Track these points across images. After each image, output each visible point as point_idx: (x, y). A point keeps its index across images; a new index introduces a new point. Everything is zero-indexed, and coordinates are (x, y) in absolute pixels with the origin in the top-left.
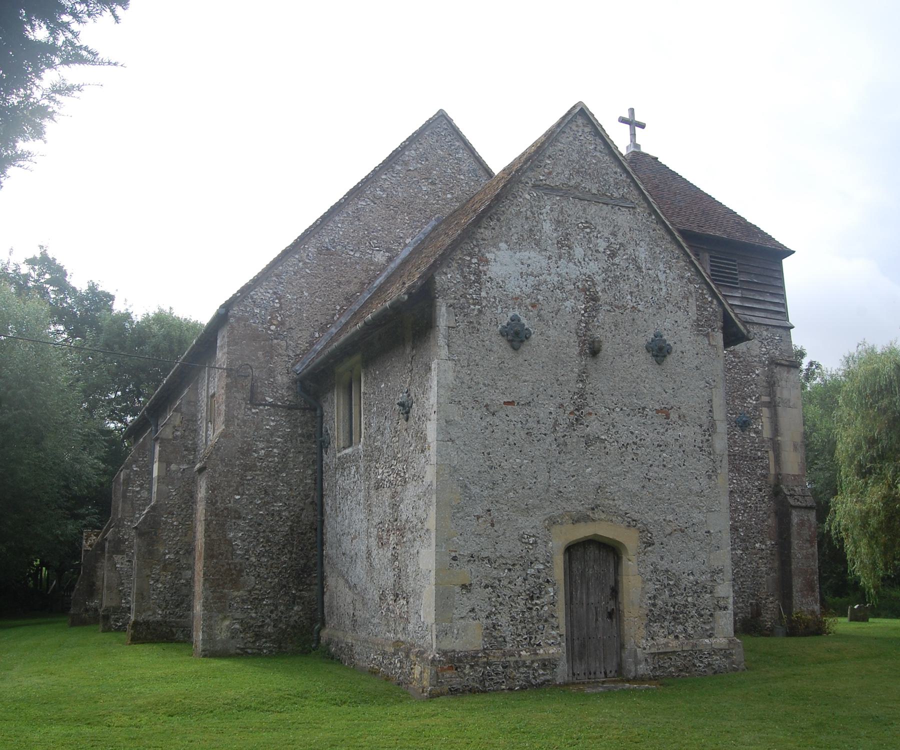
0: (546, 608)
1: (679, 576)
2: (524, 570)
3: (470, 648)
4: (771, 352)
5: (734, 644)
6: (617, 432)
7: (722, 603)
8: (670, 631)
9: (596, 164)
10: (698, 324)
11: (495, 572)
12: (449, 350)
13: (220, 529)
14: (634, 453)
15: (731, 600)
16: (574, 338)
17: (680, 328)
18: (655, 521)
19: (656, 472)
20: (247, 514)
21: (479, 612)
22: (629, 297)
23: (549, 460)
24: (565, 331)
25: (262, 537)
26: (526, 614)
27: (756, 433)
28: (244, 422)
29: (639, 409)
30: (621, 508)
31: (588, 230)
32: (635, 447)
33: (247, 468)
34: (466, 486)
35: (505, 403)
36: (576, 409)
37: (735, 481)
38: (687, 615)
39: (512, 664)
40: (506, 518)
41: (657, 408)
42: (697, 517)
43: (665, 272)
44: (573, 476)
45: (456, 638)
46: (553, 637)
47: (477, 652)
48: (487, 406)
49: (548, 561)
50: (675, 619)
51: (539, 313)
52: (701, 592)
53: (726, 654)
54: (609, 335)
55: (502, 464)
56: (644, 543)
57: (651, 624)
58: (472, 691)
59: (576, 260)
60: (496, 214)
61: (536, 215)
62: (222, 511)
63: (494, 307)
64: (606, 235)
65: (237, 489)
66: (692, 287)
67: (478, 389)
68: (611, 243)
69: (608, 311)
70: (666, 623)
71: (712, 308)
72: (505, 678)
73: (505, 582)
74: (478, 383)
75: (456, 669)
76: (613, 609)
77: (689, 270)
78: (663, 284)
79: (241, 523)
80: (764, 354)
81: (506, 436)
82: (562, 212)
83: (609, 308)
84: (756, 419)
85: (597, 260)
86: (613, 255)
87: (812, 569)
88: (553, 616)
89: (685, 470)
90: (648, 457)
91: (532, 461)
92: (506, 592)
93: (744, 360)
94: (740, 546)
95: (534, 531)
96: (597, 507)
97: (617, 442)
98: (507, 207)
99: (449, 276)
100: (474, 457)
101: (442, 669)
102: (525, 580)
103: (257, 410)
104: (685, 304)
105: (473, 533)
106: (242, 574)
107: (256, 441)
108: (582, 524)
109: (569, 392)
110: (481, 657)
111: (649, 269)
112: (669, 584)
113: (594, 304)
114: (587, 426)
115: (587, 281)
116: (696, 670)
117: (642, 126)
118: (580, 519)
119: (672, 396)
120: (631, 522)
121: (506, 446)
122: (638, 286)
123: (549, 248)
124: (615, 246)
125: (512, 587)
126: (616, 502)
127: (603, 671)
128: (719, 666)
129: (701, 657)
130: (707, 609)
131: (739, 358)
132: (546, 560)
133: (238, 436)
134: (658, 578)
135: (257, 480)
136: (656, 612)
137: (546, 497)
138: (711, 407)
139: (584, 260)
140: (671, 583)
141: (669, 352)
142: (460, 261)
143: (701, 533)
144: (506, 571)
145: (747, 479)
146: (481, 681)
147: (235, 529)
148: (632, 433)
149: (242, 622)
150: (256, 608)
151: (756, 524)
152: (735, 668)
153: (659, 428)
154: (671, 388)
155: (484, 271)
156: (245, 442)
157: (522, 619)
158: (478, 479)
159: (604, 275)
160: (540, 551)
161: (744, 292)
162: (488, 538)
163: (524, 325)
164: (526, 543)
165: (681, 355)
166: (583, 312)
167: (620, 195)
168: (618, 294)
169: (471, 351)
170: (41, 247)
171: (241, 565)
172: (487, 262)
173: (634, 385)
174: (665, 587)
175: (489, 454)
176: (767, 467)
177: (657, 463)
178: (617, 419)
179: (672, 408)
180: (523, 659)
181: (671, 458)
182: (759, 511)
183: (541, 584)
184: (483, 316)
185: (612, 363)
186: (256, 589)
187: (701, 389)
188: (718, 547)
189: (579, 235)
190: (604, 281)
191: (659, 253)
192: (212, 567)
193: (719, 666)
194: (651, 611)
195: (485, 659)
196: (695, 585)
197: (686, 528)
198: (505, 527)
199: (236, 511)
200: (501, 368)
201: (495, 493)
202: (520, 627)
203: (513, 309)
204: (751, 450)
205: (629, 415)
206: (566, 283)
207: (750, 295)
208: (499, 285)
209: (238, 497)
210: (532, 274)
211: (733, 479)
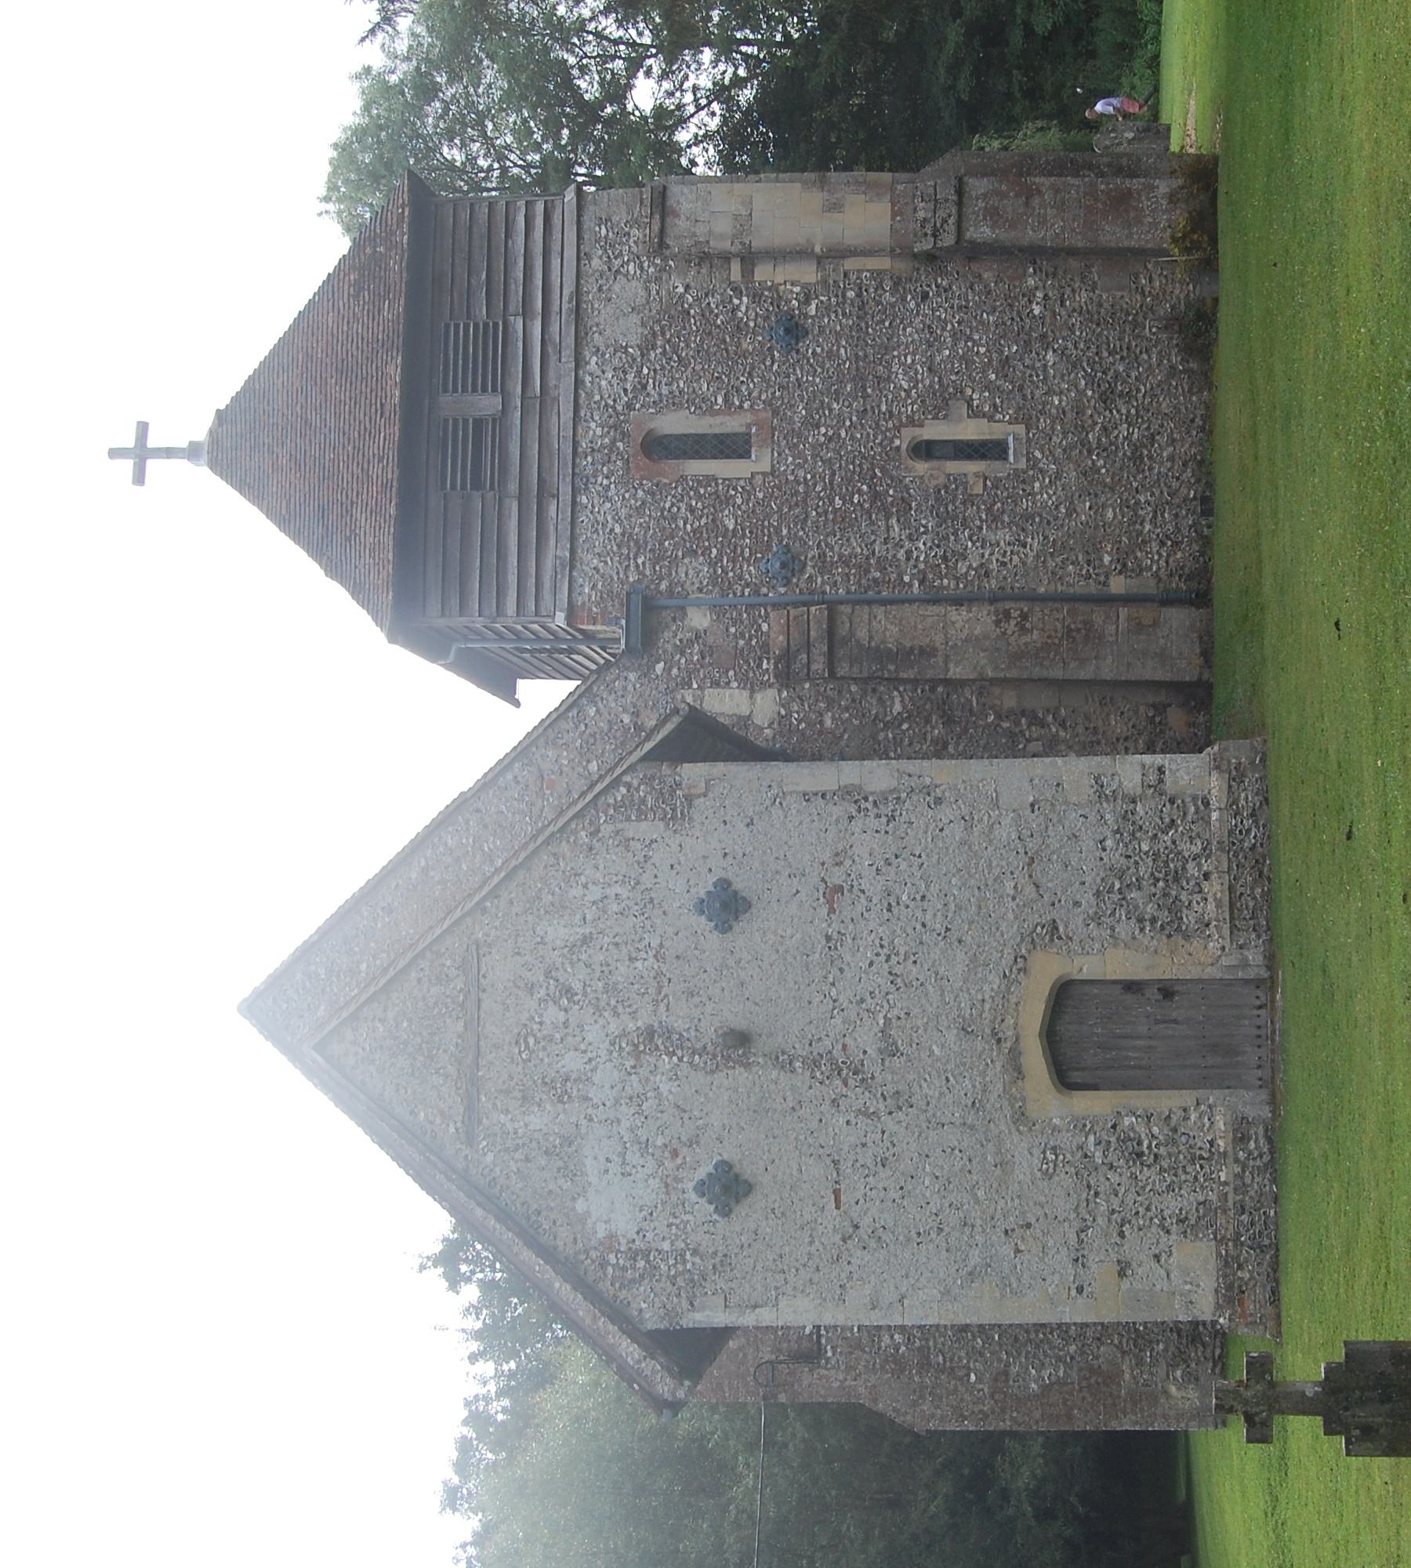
0: (1156, 1130)
1: (1105, 869)
2: (1096, 1169)
3: (1212, 1264)
4: (634, 249)
5: (1222, 759)
6: (871, 993)
7: (1152, 778)
8: (1197, 889)
9: (410, 1021)
10: (672, 818)
11: (1100, 1220)
12: (762, 1306)
13: (1026, 1404)
14: (904, 960)
15: (1148, 759)
16: (719, 1077)
17: (682, 859)
18: (1016, 918)
19: (935, 915)
20: (1000, 1360)
21: (1161, 1246)
22: (639, 964)
23: (924, 1125)
24: (711, 1094)
25: (1037, 1336)
26: (1165, 1163)
27: (807, 302)
28: (849, 1368)
29: (830, 948)
30: (995, 987)
31: (531, 1041)
32: (894, 959)
33: (925, 1364)
34: (971, 1274)
35: (838, 1207)
36: (839, 1074)
37: (909, 361)
38: (1171, 852)
39: (1238, 1198)
40: (1017, 1201)
41: (826, 911)
42: (1006, 831)
43: (585, 886)
44: (947, 1080)
45: (1198, 1286)
46: (1200, 1117)
47: (1219, 1254)
48: (844, 1240)
49: (1081, 1125)
50: (1176, 879)
51: (685, 1145)
52: (1134, 823)
53: (1236, 778)
54: (709, 1008)
55: (934, 1211)
56: (1052, 940)
57: (1184, 927)
58: (1275, 1266)
59: (587, 1067)
60: (528, 1218)
61: (520, 1142)
62: (996, 1402)
63: (685, 1227)
64: (534, 1004)
65: (960, 1379)
66: (607, 830)
67: (820, 1255)
68: (548, 995)
69: (668, 1010)
70: (1184, 897)
71: (639, 785)
72: (1260, 1209)
73: (1115, 1204)
74: (809, 1254)
75: (1243, 1292)
76: (1159, 989)
77: (575, 832)
78: (608, 891)
79: (1014, 1370)
80: (642, 268)
81: (890, 1204)
82: (507, 1092)
83: (662, 1007)
84: (780, 297)
85: (581, 1026)
86: (568, 992)
87: (1085, 194)
88: (1169, 1117)
89: (928, 856)
90: (910, 930)
91: (927, 1156)
92: (1129, 1200)
93: (659, 321)
94: (1038, 355)
95: (1036, 1152)
96: (996, 1034)
97: (887, 994)
98: (515, 1197)
99: (644, 1306)
100: (924, 1260)
101: (1243, 1315)
102: (1111, 1167)
103: (829, 1347)
104: (639, 846)
105: (1042, 1259)
106: (1096, 1367)
107: (879, 1349)
108: (1023, 1060)
109: (811, 1088)
110: (1227, 1251)
111: (584, 919)
112: (1120, 891)
113: (659, 1036)
114: (865, 1052)
115: (620, 1047)
116: (1262, 845)
117: (143, 429)
118: (1016, 1069)
119: (803, 879)
120: (1019, 966)
121: (905, 1203)
122: (617, 944)
123: (573, 1119)
124: (552, 987)
125: (1123, 1190)
126: (987, 997)
127: (1256, 1012)
128: (1257, 794)
129: (1240, 831)
130: (1162, 811)
131: (654, 335)
132: (1081, 1131)
133: (873, 1379)
134: (1109, 912)
135: (943, 1345)
136: (1164, 916)
137: (984, 1129)
138: (816, 794)
139: (584, 1052)
140: (1117, 886)
141: (724, 884)
142: (617, 1285)
143: (1035, 821)
144: (1098, 1200)
145: (904, 329)
146: (1262, 1251)
147: (1024, 1380)
148: (871, 964)
149: (1172, 1366)
150: (1151, 1342)
151: (994, 310)
152: (1261, 759)
153: (859, 908)
154: (789, 881)
155: (628, 1242)
156: (882, 1367)
157: (1172, 1173)
158: (959, 1253)
159: (606, 1014)
160: (1067, 1140)
161: (512, 309)
162: (1048, 1232)
163: (710, 1175)
164: (1055, 1165)
165: (729, 859)
166: (675, 1059)
167: (458, 976)
168: (636, 986)
169: (759, 1268)
170: (422, 1268)
171: (1081, 1370)
172: (612, 1236)
173: (789, 959)
174: (1124, 899)
175: (919, 1234)
176: (877, 275)
177: (919, 914)
178: (849, 993)
179: (823, 880)
180: (1231, 1179)
181: (909, 885)
182: (967, 301)
183: (1118, 1139)
184: (701, 1248)
185: (756, 1004)
186: (1120, 1343)
187: (786, 817)
188: (1058, 785)
189: (542, 1060)
190: (616, 1014)
191: (553, 894)
192: (1086, 1416)
193: (1257, 794)
194: (1162, 927)
195: (1230, 1244)
196: (1122, 835)
197: (1026, 853)
198: (1031, 1204)
199: (996, 1380)
200: (783, 1214)
201: (979, 1222)
202: (1183, 1177)
203: (684, 1192)
204: (844, 314)
205: (841, 970)
206: (629, 1091)
207: (517, 292)
208: (648, 1217)
209: (973, 1377)
210: (623, 1155)
211: (904, 364)
